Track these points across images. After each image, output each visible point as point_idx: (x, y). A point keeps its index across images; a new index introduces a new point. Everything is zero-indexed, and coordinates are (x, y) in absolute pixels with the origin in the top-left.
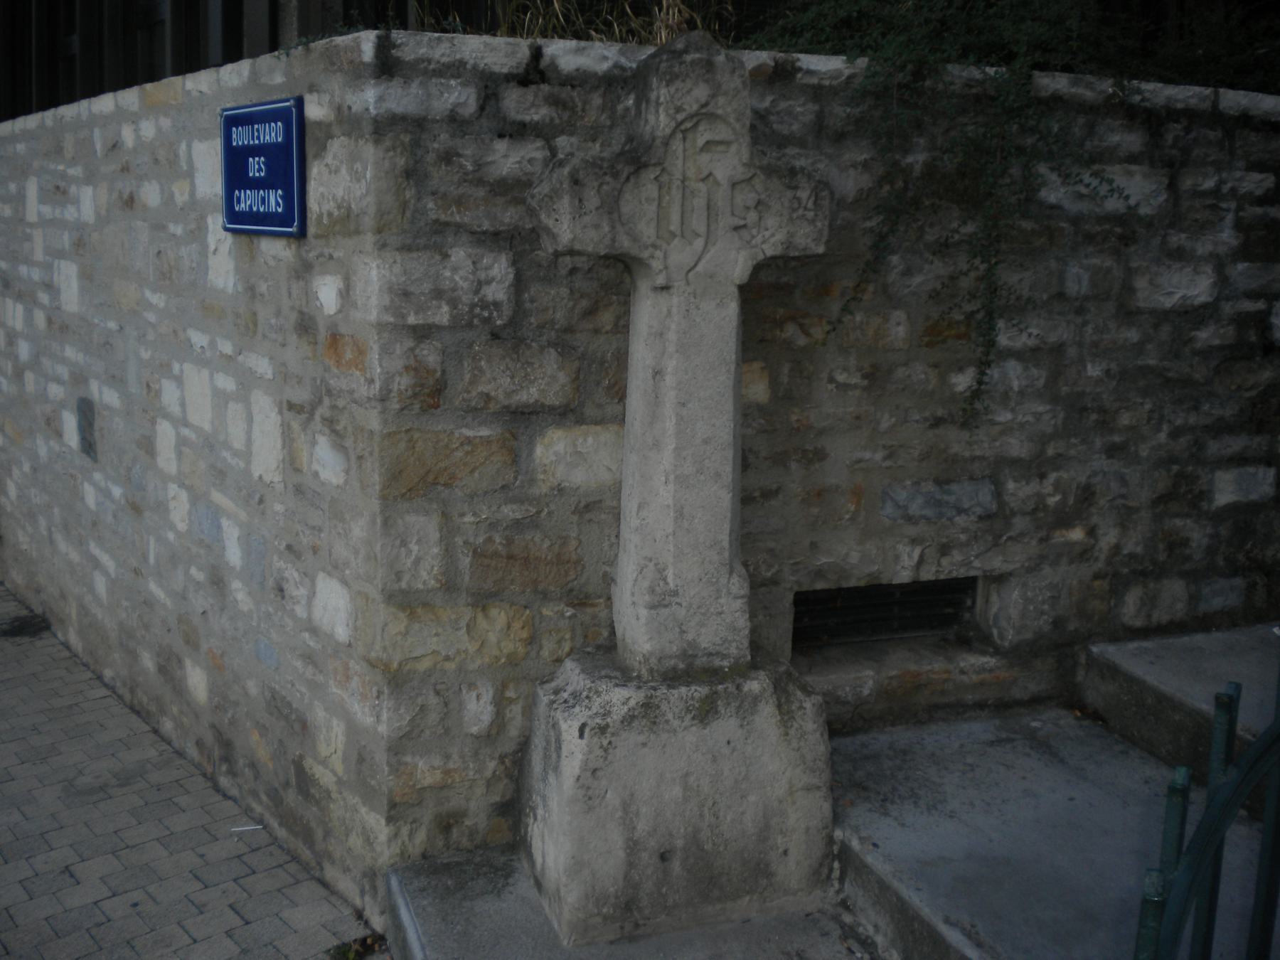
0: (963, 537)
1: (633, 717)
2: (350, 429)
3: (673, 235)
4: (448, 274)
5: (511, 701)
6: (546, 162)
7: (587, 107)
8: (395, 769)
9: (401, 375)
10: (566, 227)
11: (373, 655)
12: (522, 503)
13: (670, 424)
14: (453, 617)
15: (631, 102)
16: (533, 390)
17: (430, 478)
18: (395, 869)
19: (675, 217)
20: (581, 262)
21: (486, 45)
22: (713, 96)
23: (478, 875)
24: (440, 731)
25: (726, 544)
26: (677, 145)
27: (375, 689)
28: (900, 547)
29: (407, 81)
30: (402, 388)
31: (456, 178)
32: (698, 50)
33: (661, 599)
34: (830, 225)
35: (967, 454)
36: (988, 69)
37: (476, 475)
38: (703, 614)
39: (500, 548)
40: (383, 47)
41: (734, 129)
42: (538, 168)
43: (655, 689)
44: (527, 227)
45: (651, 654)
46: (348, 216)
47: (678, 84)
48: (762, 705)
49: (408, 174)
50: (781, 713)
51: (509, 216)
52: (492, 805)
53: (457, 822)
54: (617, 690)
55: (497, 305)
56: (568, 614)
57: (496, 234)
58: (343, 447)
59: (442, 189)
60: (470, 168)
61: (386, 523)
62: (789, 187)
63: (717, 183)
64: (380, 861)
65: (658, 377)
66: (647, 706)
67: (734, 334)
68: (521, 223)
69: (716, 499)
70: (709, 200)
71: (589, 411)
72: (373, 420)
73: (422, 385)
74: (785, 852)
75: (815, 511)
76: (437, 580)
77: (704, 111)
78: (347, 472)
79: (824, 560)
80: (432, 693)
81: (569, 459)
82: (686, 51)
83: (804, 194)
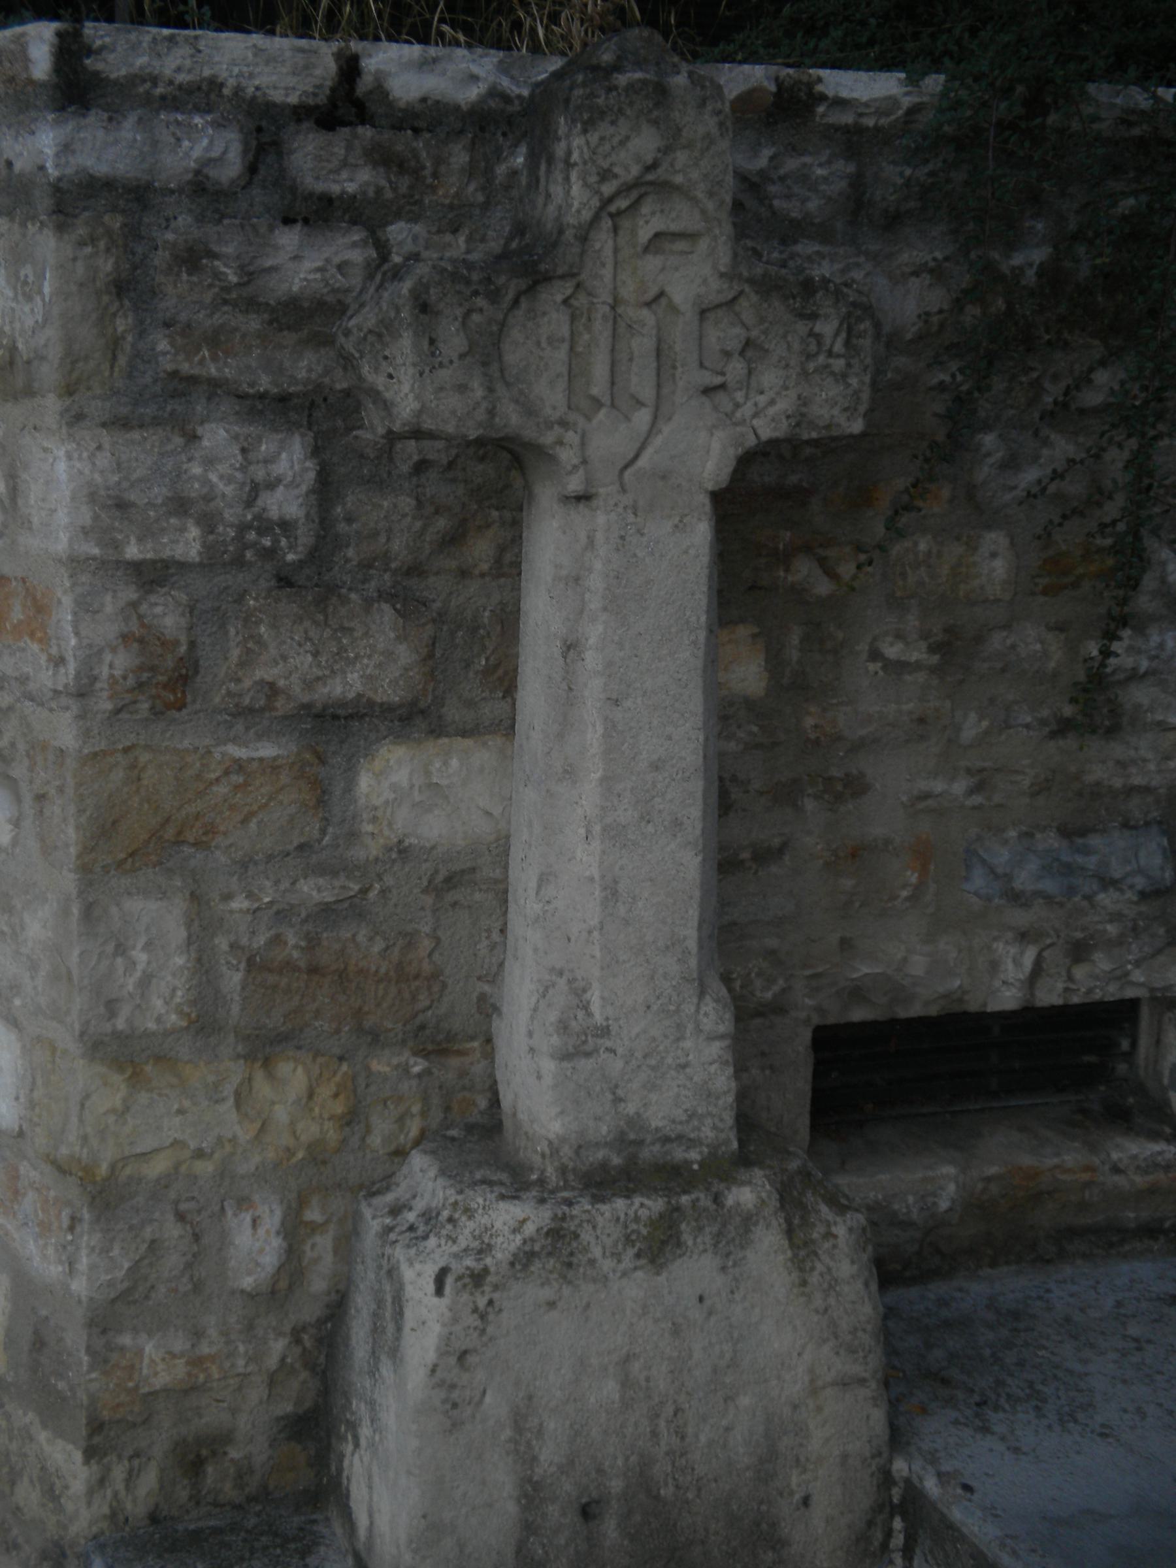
0: (1112, 929)
1: (531, 1255)
2: (21, 746)
3: (597, 403)
4: (197, 470)
5: (314, 1228)
6: (371, 270)
7: (443, 169)
8: (101, 1359)
9: (114, 650)
10: (408, 388)
11: (64, 1151)
12: (335, 874)
13: (593, 737)
14: (211, 1078)
15: (520, 160)
16: (353, 677)
17: (170, 833)
18: (99, 1543)
19: (600, 370)
20: (435, 450)
21: (258, 51)
22: (667, 150)
23: (252, 1551)
24: (185, 1286)
25: (692, 944)
26: (603, 240)
27: (65, 1215)
28: (999, 946)
29: (114, 116)
30: (117, 673)
31: (208, 297)
32: (639, 64)
33: (580, 1043)
34: (874, 383)
35: (1118, 783)
36: (1161, 91)
37: (253, 825)
38: (653, 1068)
39: (296, 954)
40: (69, 52)
41: (703, 212)
42: (356, 280)
43: (570, 1203)
44: (338, 387)
45: (563, 1140)
46: (12, 363)
47: (604, 128)
48: (759, 1231)
49: (121, 287)
50: (792, 1245)
51: (305, 367)
52: (278, 1419)
53: (214, 1453)
54: (502, 1205)
55: (286, 526)
56: (416, 1069)
57: (283, 398)
58: (8, 777)
59: (183, 317)
60: (233, 279)
61: (89, 913)
62: (801, 316)
63: (673, 309)
64: (74, 1529)
65: (572, 653)
66: (557, 1234)
67: (704, 580)
68: (327, 380)
69: (677, 862)
70: (659, 340)
71: (453, 712)
72: (64, 731)
73: (153, 669)
74: (806, 1501)
75: (848, 883)
76: (181, 1013)
77: (650, 177)
78: (17, 823)
79: (865, 970)
80: (170, 1217)
81: (417, 797)
82: (616, 68)
83: (827, 328)
